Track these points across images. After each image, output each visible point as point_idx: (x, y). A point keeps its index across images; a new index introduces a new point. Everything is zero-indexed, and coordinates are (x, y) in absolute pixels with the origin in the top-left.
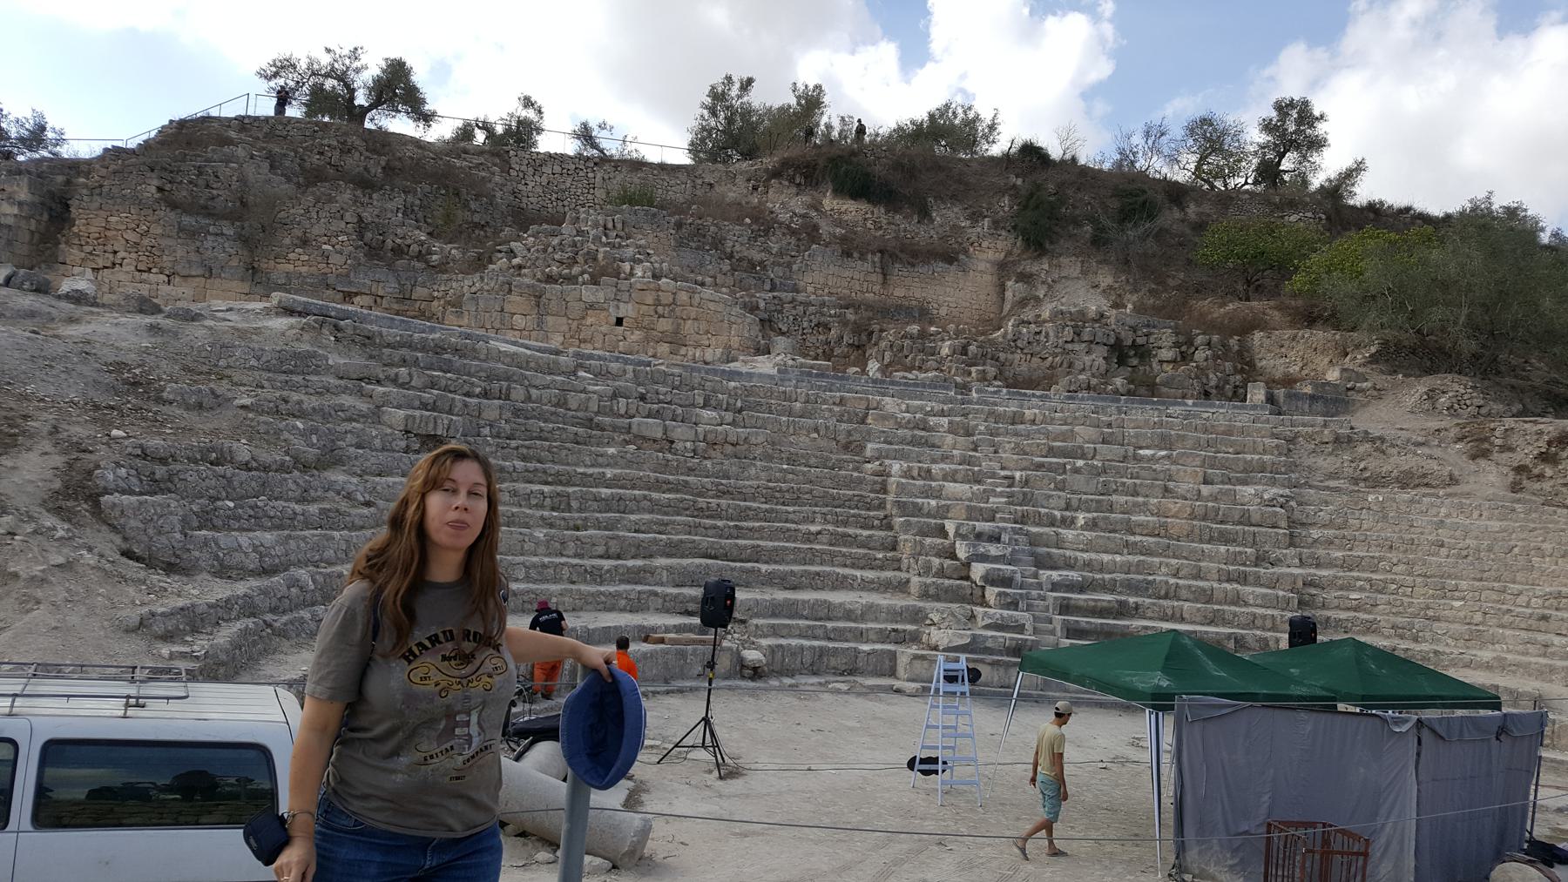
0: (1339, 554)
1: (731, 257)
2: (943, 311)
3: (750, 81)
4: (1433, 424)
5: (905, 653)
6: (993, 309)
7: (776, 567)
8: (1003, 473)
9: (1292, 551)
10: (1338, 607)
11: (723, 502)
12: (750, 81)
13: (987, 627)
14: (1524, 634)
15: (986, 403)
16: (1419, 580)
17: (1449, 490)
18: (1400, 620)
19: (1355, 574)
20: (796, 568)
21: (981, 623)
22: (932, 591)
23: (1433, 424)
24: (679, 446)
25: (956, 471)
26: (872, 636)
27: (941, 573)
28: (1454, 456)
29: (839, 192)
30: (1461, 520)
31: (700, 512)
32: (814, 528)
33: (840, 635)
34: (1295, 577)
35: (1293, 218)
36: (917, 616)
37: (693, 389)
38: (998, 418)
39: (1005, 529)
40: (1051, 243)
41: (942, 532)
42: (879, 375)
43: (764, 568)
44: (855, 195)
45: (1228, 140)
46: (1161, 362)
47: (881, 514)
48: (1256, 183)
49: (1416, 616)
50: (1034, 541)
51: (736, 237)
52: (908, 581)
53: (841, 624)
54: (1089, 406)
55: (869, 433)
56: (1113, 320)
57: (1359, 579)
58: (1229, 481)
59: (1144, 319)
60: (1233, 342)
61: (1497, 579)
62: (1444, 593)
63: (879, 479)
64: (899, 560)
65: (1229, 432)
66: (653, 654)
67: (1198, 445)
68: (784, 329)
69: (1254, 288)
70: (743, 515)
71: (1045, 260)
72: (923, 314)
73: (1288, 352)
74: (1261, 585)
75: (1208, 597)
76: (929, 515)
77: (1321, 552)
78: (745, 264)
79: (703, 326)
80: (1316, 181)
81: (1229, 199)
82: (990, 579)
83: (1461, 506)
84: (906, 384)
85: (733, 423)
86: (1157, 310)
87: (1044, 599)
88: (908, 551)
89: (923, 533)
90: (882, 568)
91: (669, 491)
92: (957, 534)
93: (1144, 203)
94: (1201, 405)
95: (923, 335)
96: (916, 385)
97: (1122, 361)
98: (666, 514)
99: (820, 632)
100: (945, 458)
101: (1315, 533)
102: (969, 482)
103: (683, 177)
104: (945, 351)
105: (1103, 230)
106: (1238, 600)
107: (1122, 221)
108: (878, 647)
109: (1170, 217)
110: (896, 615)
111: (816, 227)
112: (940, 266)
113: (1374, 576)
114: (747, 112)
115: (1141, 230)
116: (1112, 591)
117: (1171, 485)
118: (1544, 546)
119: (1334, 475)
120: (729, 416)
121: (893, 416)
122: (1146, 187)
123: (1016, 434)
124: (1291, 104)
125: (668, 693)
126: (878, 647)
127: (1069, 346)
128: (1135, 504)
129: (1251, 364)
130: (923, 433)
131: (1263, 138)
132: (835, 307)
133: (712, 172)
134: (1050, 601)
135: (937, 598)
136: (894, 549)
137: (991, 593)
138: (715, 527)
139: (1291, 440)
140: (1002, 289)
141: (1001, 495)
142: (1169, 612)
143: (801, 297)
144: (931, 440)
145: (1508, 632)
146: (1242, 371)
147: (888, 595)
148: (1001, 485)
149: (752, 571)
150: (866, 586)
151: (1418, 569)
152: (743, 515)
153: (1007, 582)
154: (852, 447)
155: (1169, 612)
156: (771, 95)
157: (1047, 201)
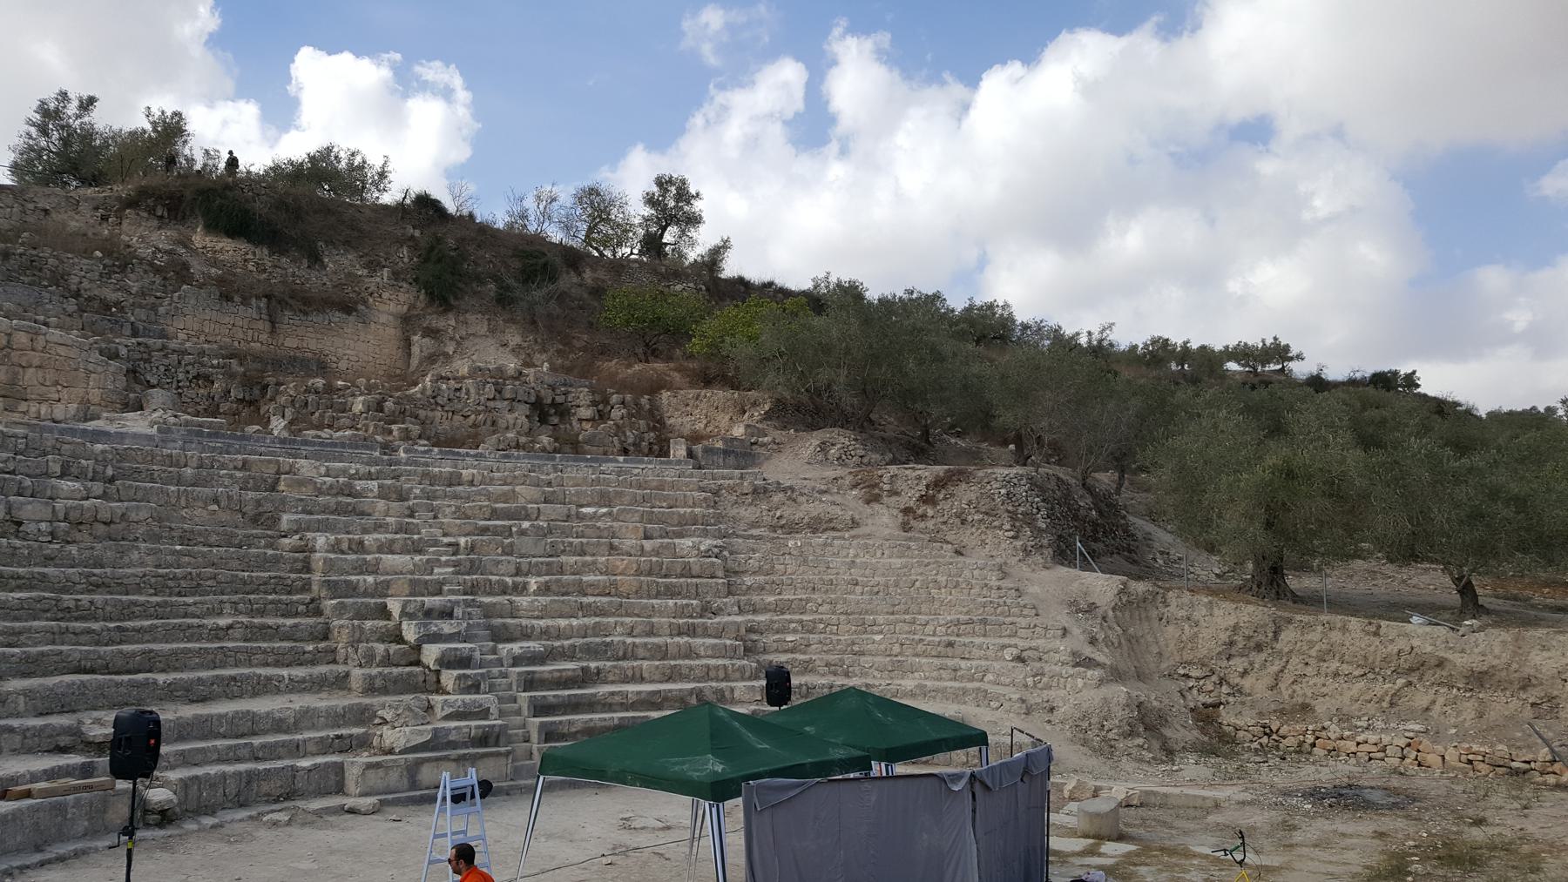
0: (771, 599)
1: (77, 295)
2: (343, 365)
3: (92, 100)
4: (830, 473)
5: (355, 763)
6: (399, 364)
7: (178, 676)
8: (446, 540)
9: (730, 600)
10: (777, 651)
11: (98, 598)
12: (92, 100)
13: (447, 718)
14: (936, 661)
15: (416, 464)
16: (843, 617)
17: (853, 532)
18: (832, 658)
19: (788, 617)
20: (204, 674)
21: (439, 713)
22: (378, 683)
23: (830, 473)
24: (30, 528)
25: (393, 541)
26: (311, 748)
27: (387, 661)
28: (851, 502)
29: (212, 227)
30: (867, 558)
31: (67, 613)
32: (223, 622)
33: (271, 752)
34: (738, 625)
35: (679, 287)
36: (363, 716)
37: (45, 454)
38: (433, 479)
39: (457, 602)
40: (456, 298)
41: (384, 613)
42: (285, 434)
43: (161, 678)
44: (232, 233)
45: (614, 211)
46: (580, 420)
47: (307, 597)
48: (641, 253)
49: (844, 652)
50: (488, 612)
51: (84, 272)
52: (347, 675)
53: (271, 739)
54: (525, 464)
55: (283, 501)
56: (531, 378)
57: (791, 621)
58: (667, 535)
59: (561, 377)
60: (644, 400)
61: (906, 612)
62: (864, 628)
63: (300, 556)
64: (334, 651)
65: (661, 487)
66: (15, 816)
67: (634, 502)
68: (154, 381)
69: (652, 353)
70: (127, 612)
71: (451, 315)
72: (322, 367)
73: (697, 411)
74: (710, 636)
75: (662, 653)
76: (366, 594)
77: (755, 598)
78: (96, 304)
79: (51, 376)
80: (693, 255)
81: (620, 266)
82: (446, 662)
83: (866, 546)
84: (321, 444)
85: (104, 496)
86: (568, 371)
87: (505, 676)
88: (345, 638)
89: (361, 615)
90: (313, 663)
91: (20, 588)
92: (404, 614)
93: (545, 265)
94: (632, 462)
95: (330, 389)
96: (334, 445)
97: (543, 420)
98: (16, 619)
99: (244, 752)
100: (379, 527)
101: (749, 580)
102: (409, 552)
103: (9, 200)
104: (358, 406)
105: (508, 288)
106: (690, 653)
107: (525, 281)
108: (320, 760)
109: (568, 280)
110: (337, 718)
111: (186, 266)
112: (337, 316)
113: (805, 618)
114: (88, 135)
115: (545, 290)
116: (572, 658)
117: (616, 541)
118: (939, 578)
119: (755, 524)
120: (98, 487)
121: (311, 481)
122: (545, 250)
123: (456, 496)
124: (670, 181)
125: (42, 864)
126: (320, 760)
127: (491, 404)
128: (585, 564)
129: (661, 422)
130: (349, 500)
131: (648, 211)
132: (216, 357)
133: (47, 197)
134: (513, 678)
135: (385, 691)
136: (326, 638)
137: (449, 678)
138: (89, 631)
139: (716, 493)
140: (408, 344)
141: (447, 564)
142: (630, 673)
143: (173, 344)
144: (360, 507)
145: (924, 660)
146: (654, 429)
147: (324, 695)
148: (446, 553)
149: (145, 684)
150: (296, 687)
151: (840, 608)
152: (127, 612)
153: (464, 662)
154: (264, 519)
155: (630, 673)
156: (124, 113)
157: (445, 255)
